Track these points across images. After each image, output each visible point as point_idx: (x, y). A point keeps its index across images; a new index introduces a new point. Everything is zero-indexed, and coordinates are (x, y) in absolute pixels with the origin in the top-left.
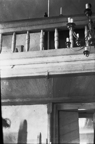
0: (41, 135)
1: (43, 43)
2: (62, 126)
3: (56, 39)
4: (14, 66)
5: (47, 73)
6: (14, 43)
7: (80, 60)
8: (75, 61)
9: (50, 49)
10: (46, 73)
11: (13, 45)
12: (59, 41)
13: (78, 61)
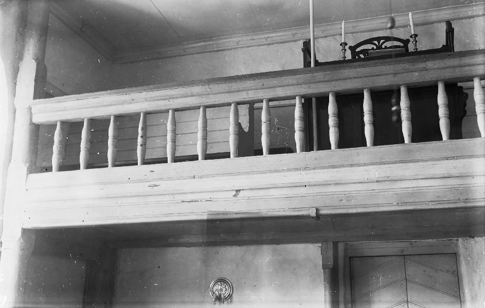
0: (153, 171)
1: (301, 132)
2: (63, 85)
3: (332, 121)
4: (238, 191)
5: (315, 211)
6: (203, 136)
7: (390, 179)
8: (377, 181)
9: (320, 148)
10: (311, 209)
11: (445, 123)
12: (341, 125)
13: (385, 181)
